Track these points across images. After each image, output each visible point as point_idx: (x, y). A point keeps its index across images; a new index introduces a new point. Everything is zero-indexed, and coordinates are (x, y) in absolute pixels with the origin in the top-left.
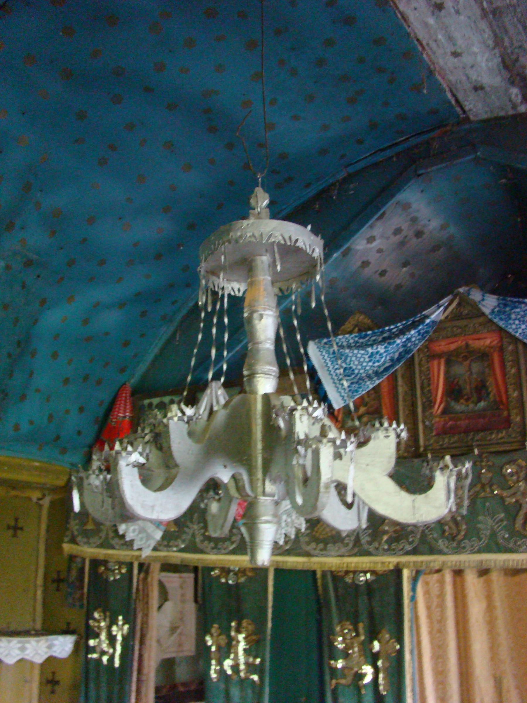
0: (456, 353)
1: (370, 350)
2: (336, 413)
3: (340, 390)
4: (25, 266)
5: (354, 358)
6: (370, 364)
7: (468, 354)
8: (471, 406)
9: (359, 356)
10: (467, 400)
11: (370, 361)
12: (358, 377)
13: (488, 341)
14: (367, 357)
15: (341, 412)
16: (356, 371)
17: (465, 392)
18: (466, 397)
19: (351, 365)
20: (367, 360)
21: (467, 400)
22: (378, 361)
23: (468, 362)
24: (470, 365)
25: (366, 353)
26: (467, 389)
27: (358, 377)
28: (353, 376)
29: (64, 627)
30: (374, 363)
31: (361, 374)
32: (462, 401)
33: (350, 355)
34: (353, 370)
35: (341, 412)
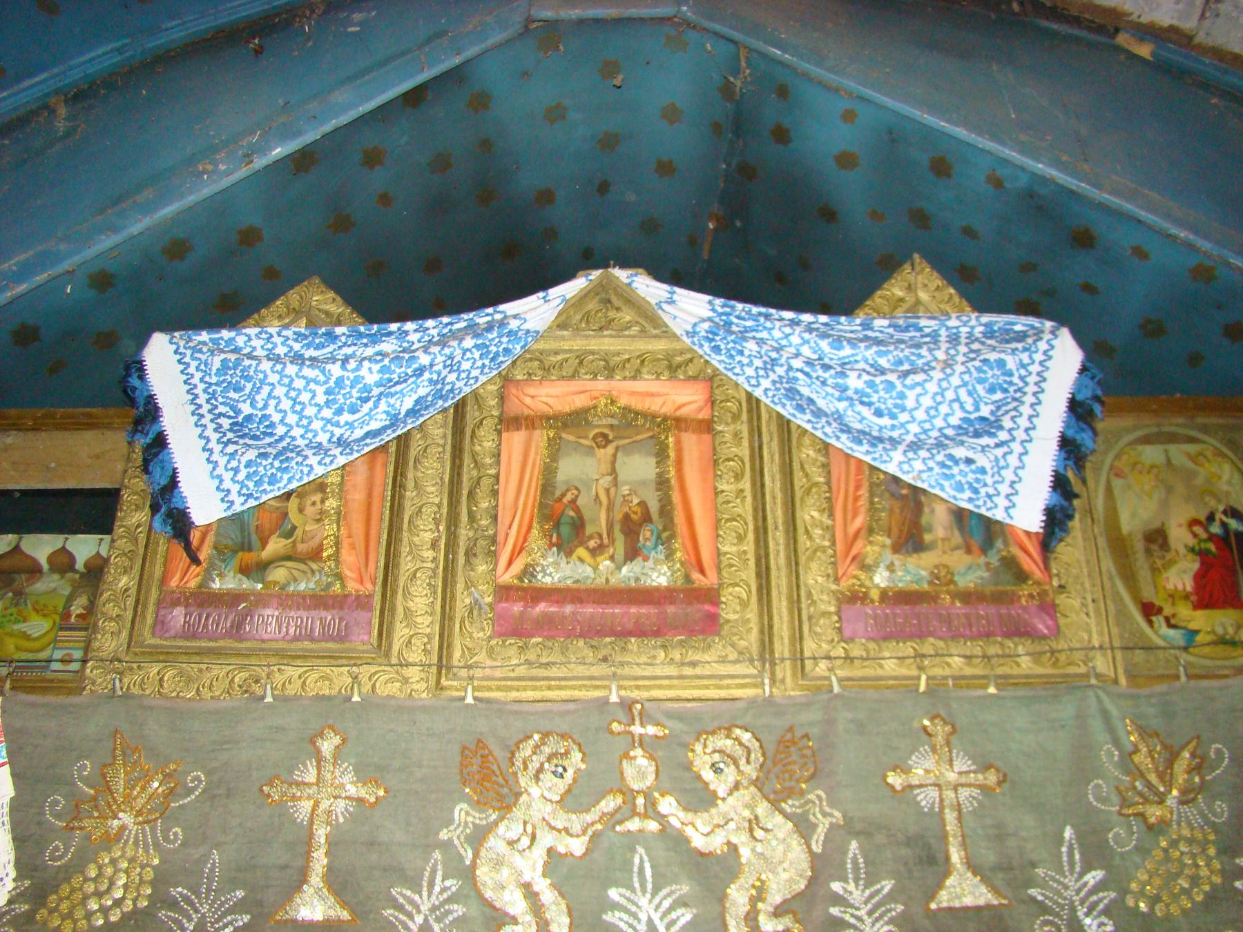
0: (574, 420)
1: (335, 370)
2: (195, 537)
3: (219, 471)
4: (785, 99)
5: (280, 391)
6: (327, 413)
7: (633, 427)
8: (605, 564)
9: (300, 383)
10: (594, 552)
11: (328, 404)
12: (284, 444)
13: (684, 398)
14: (320, 390)
15: (210, 539)
16: (280, 430)
17: (589, 530)
18: (592, 544)
19: (270, 410)
20: (321, 399)
21: (594, 552)
22: (353, 410)
23: (610, 449)
24: (615, 456)
25: (322, 378)
26: (598, 522)
27: (284, 444)
28: (268, 440)
29: (575, 791)
30: (339, 412)
31: (294, 439)
32: (581, 552)
33: (273, 378)
34: (272, 425)
35: (210, 539)
